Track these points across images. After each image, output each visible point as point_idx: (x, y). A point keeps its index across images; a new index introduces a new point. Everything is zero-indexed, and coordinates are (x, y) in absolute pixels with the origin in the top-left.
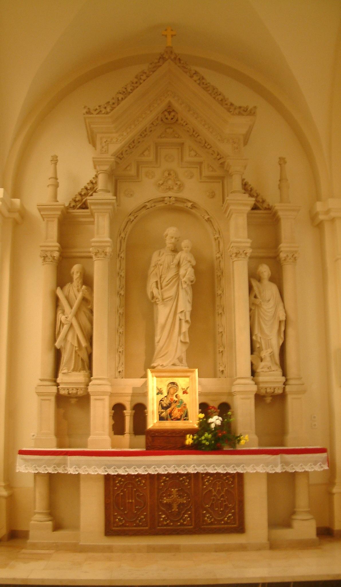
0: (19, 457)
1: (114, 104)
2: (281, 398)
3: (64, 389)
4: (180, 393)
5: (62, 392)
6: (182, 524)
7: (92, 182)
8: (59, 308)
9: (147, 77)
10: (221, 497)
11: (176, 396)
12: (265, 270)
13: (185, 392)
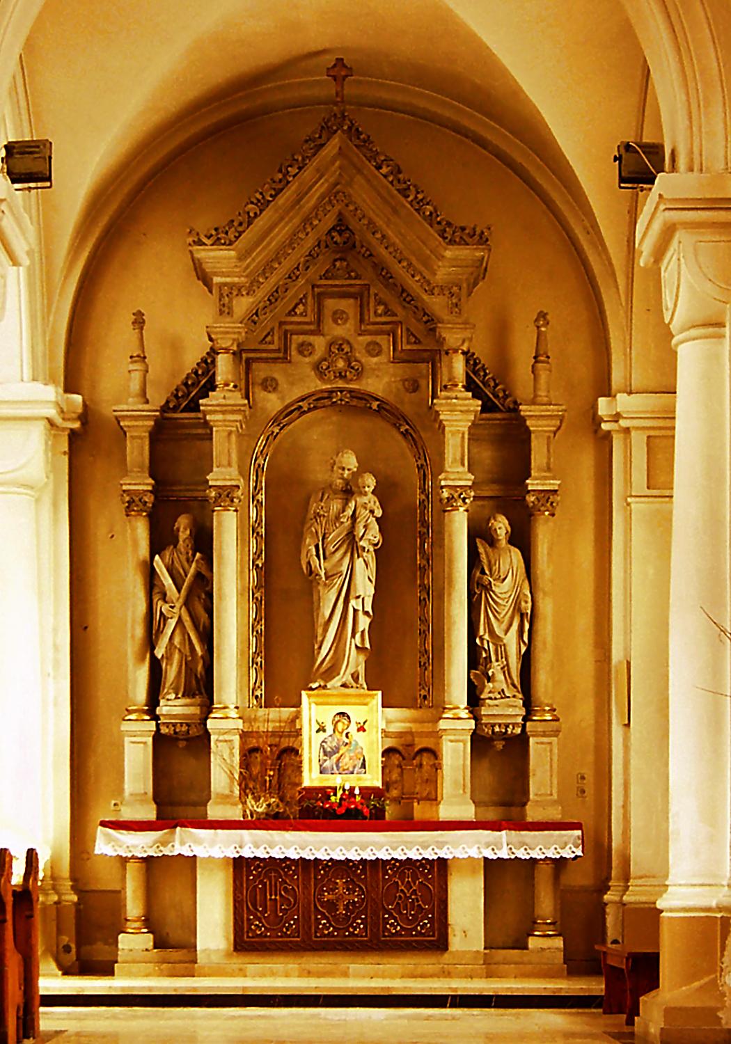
0: (100, 828)
1: (241, 224)
2: (518, 745)
3: (167, 725)
4: (353, 729)
5: (164, 730)
6: (352, 934)
7: (204, 361)
8: (156, 590)
9: (300, 169)
10: (412, 894)
11: (347, 736)
12: (501, 526)
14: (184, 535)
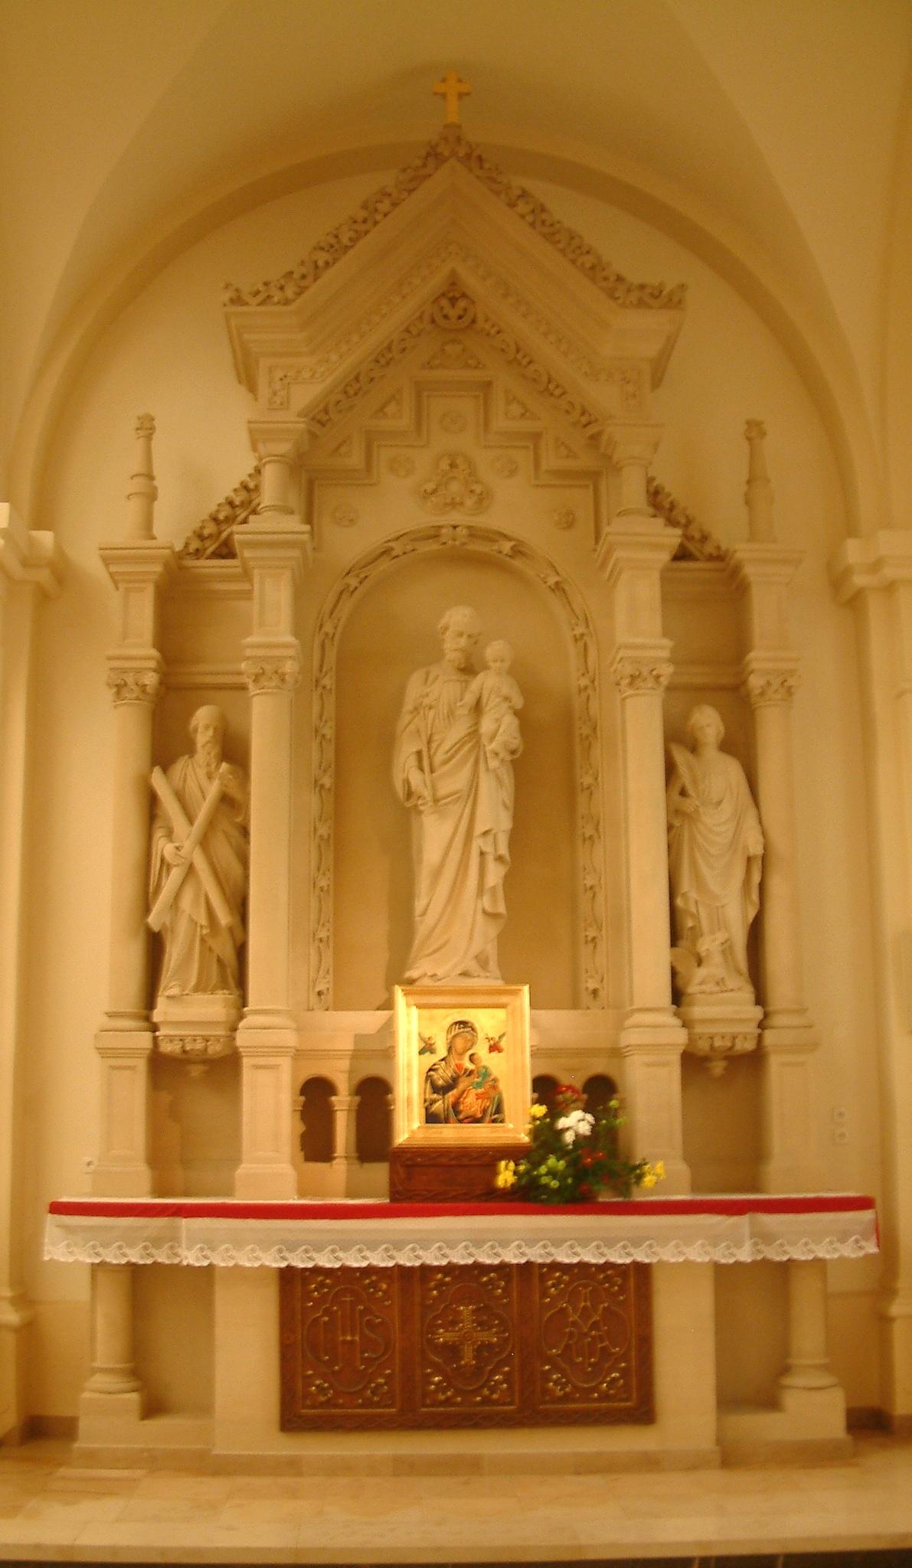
0: (51, 1220)
1: (304, 277)
2: (750, 1063)
3: (171, 1039)
4: (481, 1050)
5: (166, 1048)
6: (487, 1401)
7: (245, 487)
8: (158, 823)
9: (394, 205)
10: (591, 1328)
11: (472, 1058)
12: (708, 722)
13: (494, 1048)
14: (203, 738)
